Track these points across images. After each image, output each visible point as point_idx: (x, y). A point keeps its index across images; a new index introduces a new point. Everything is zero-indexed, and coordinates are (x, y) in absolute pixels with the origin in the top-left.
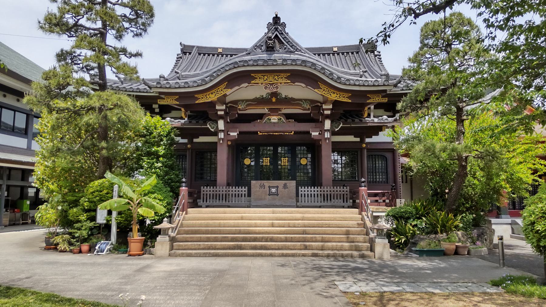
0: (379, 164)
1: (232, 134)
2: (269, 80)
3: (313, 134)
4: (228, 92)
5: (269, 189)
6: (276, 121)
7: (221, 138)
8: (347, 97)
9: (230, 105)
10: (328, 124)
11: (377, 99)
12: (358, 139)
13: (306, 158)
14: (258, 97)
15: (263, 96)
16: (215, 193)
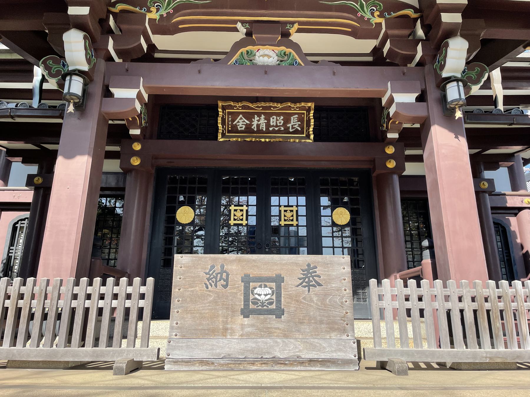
1: (119, 93)
13: (334, 224)
16: (93, 305)
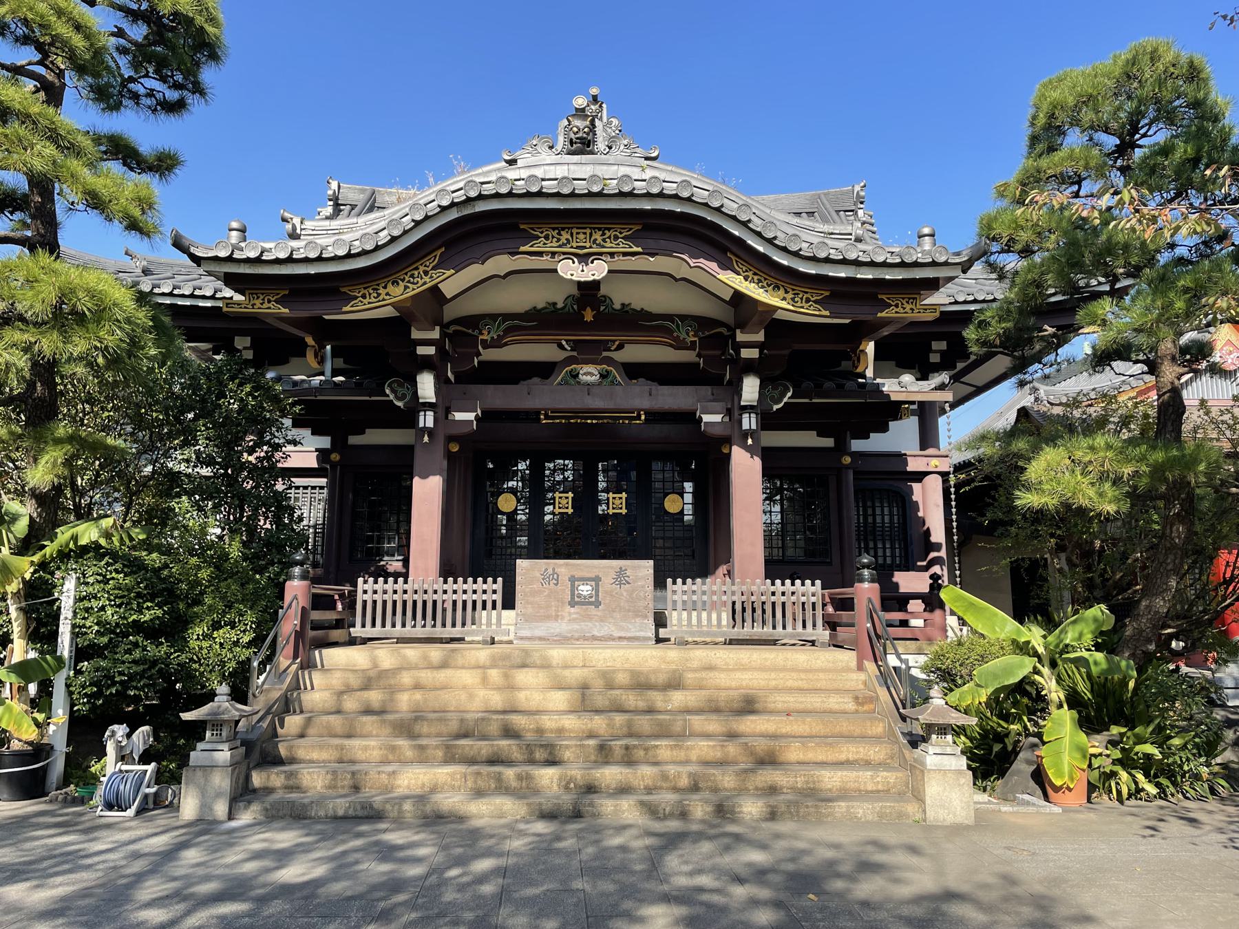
0: (883, 515)
1: (459, 416)
2: (575, 245)
3: (707, 418)
4: (452, 283)
5: (573, 586)
6: (595, 378)
7: (425, 428)
8: (815, 302)
9: (453, 328)
10: (750, 389)
11: (908, 307)
12: (829, 442)
14: (540, 306)
15: (555, 304)
